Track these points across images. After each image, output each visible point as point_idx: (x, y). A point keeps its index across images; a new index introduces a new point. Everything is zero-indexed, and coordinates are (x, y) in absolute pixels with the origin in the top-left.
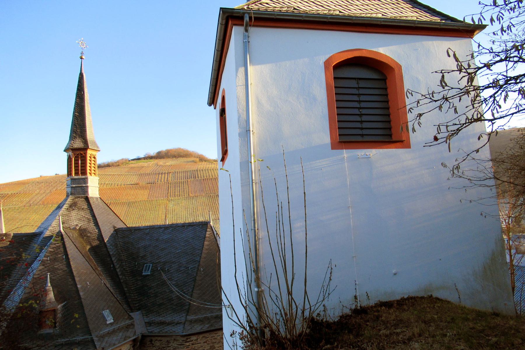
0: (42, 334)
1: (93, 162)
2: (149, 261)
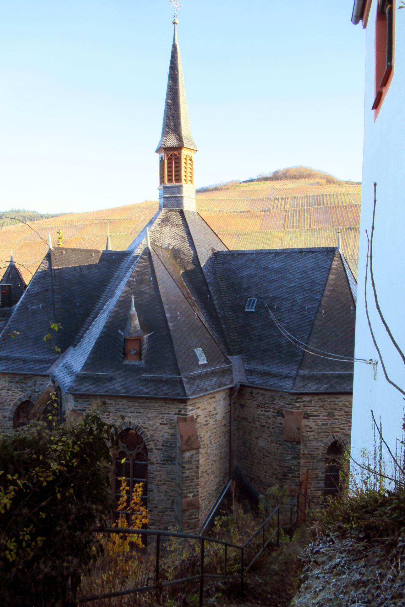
2: (253, 294)
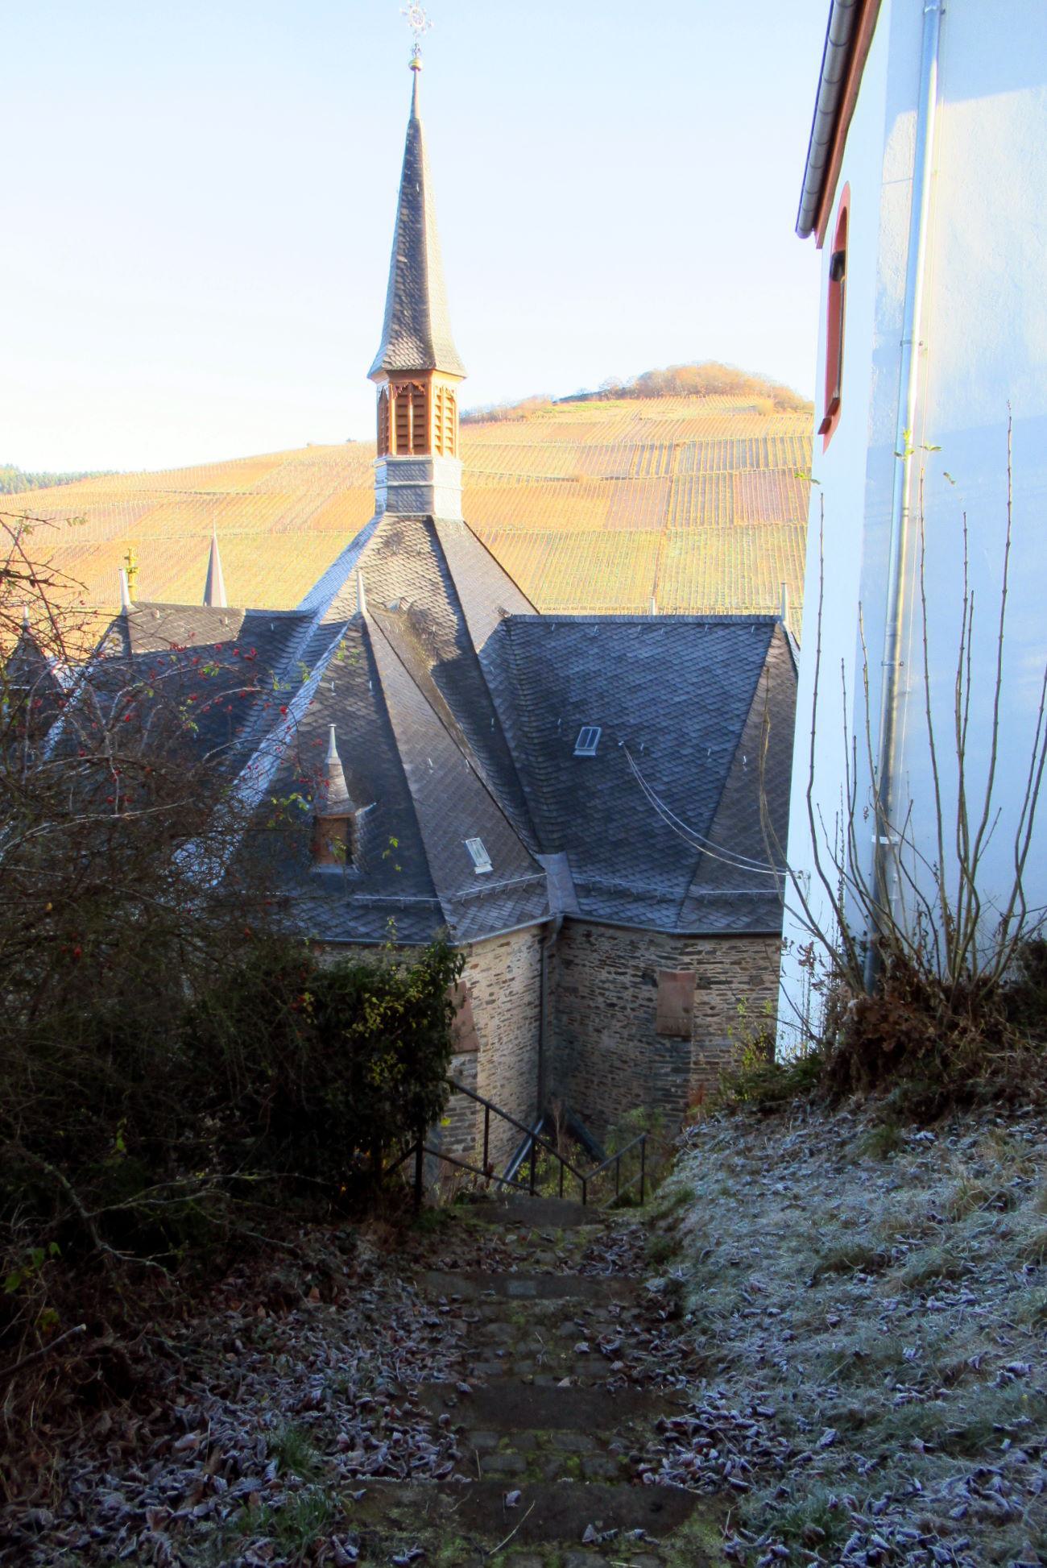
0: (320, 875)
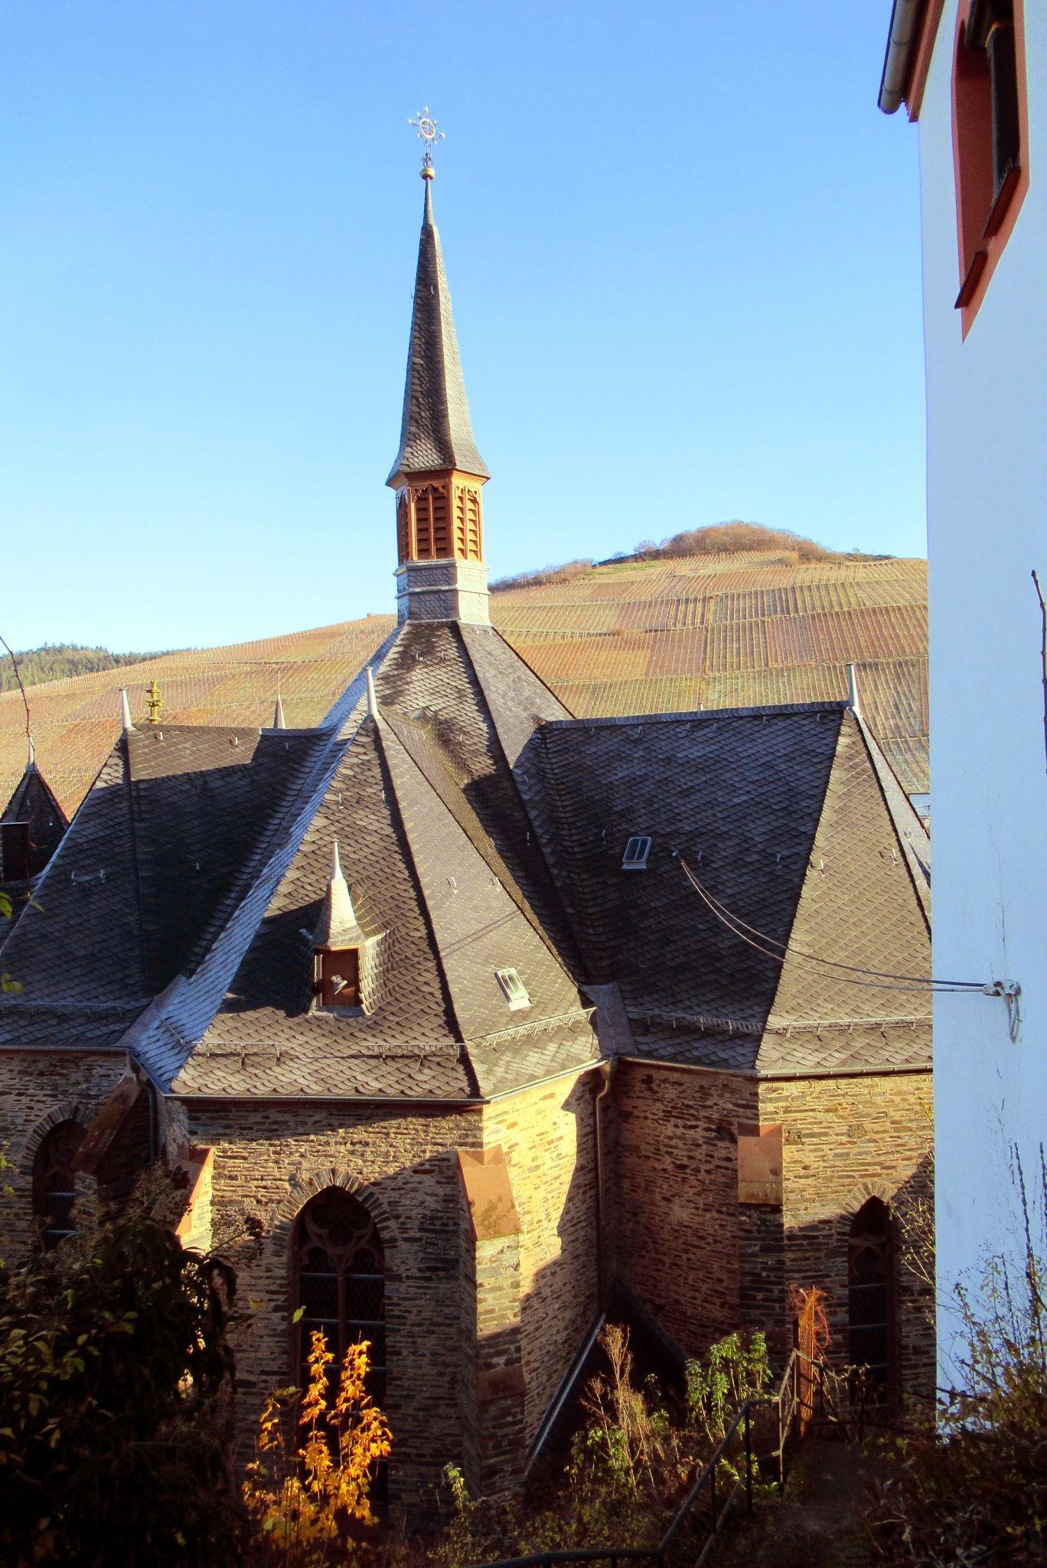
1: (469, 515)
